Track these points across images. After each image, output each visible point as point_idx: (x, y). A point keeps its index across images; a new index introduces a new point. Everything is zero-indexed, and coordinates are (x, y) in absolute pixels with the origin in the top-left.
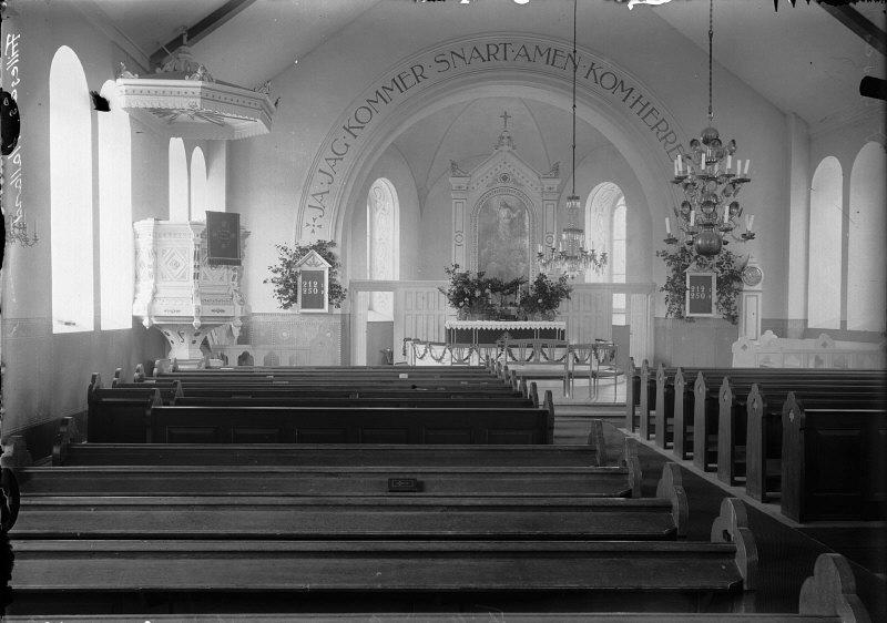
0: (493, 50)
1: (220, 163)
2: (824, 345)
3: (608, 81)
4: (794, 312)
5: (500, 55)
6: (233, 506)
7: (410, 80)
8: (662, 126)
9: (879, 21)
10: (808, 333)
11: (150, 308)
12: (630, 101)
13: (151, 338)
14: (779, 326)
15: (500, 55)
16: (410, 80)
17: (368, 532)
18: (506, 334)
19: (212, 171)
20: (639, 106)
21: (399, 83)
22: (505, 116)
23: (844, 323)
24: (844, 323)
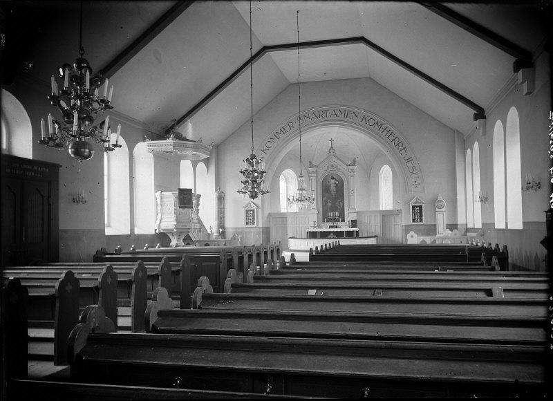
0: (321, 113)
1: (213, 168)
2: (455, 235)
3: (371, 122)
4: (461, 220)
5: (324, 115)
6: (264, 287)
7: (287, 129)
8: (397, 140)
9: (163, 6)
10: (468, 230)
11: (159, 226)
12: (382, 130)
13: (163, 237)
14: (453, 227)
15: (324, 115)
16: (287, 129)
17: (123, 314)
18: (332, 234)
19: (210, 171)
20: (385, 132)
21: (283, 130)
22: (332, 140)
23: (132, 230)
24: (132, 230)
